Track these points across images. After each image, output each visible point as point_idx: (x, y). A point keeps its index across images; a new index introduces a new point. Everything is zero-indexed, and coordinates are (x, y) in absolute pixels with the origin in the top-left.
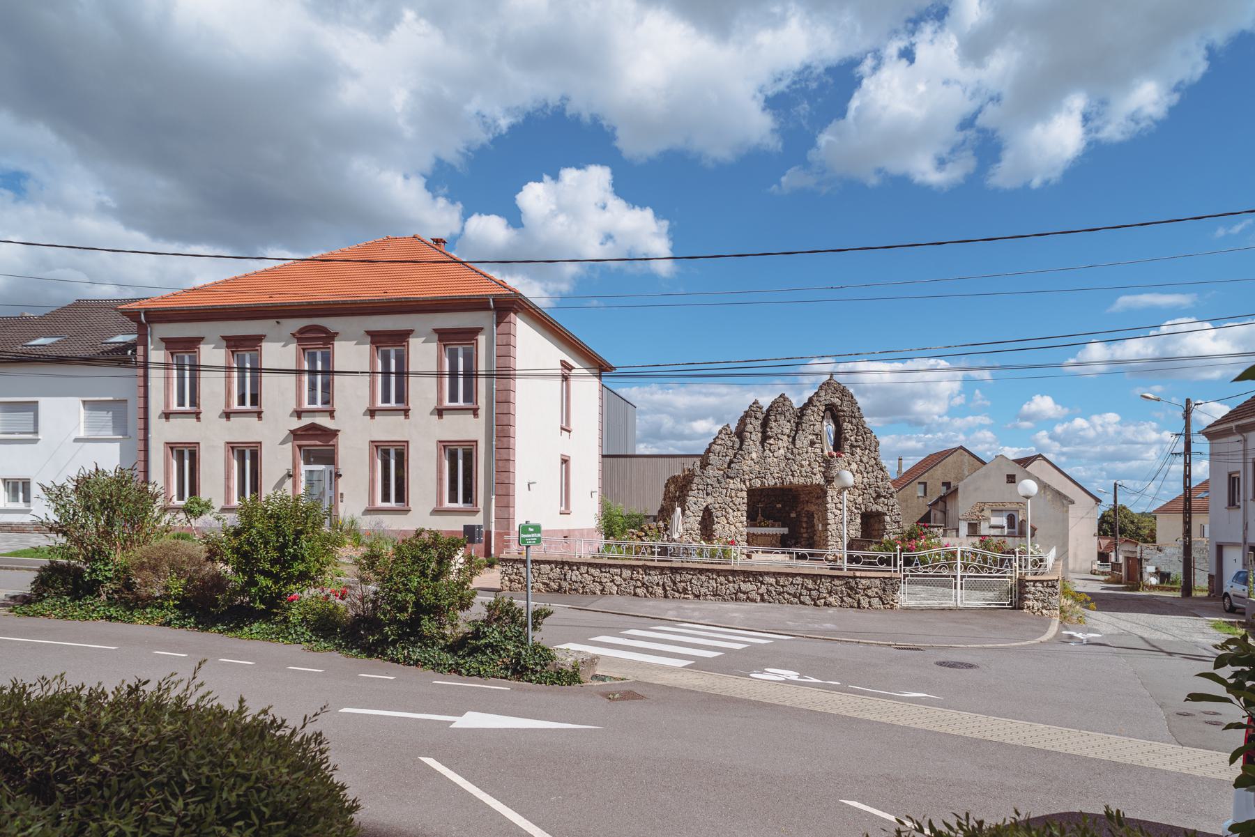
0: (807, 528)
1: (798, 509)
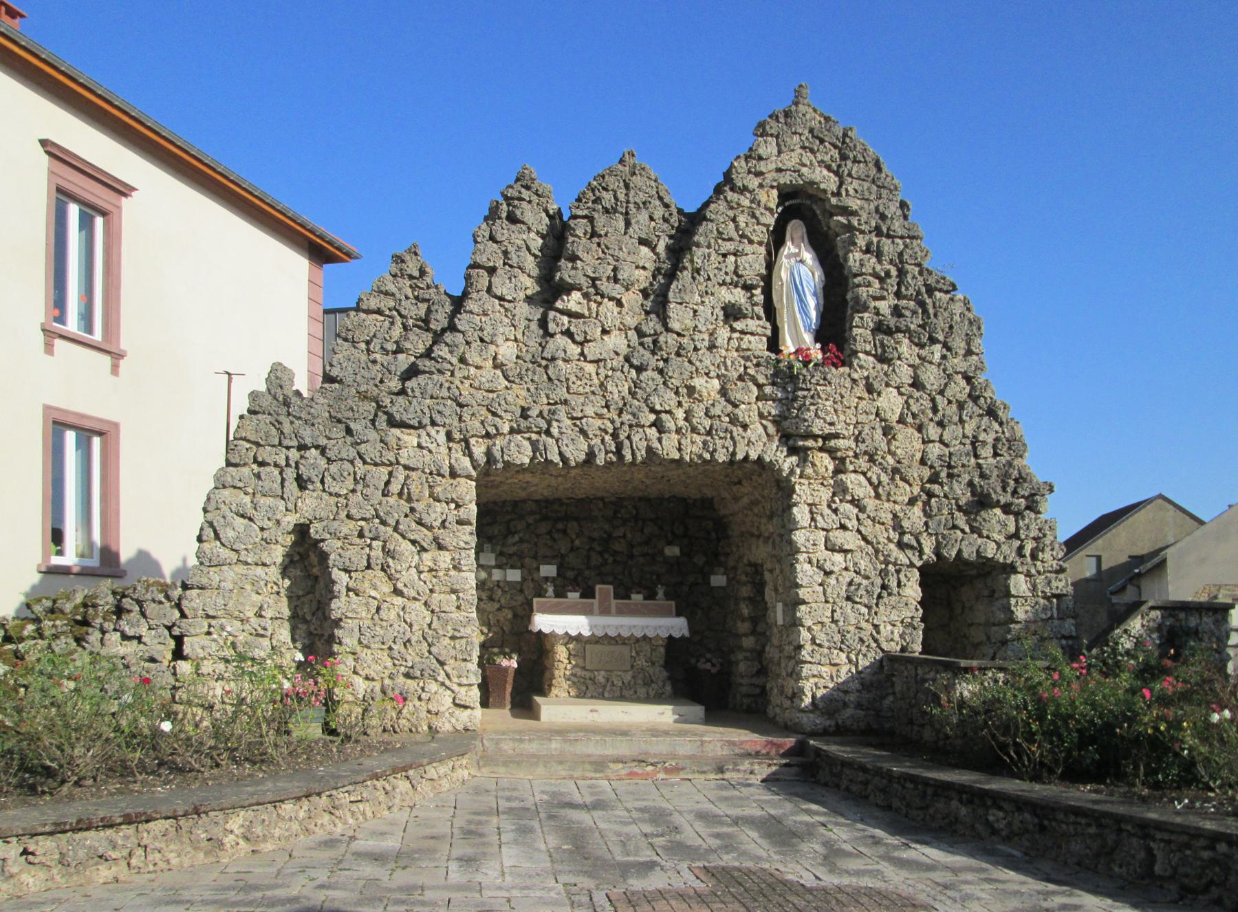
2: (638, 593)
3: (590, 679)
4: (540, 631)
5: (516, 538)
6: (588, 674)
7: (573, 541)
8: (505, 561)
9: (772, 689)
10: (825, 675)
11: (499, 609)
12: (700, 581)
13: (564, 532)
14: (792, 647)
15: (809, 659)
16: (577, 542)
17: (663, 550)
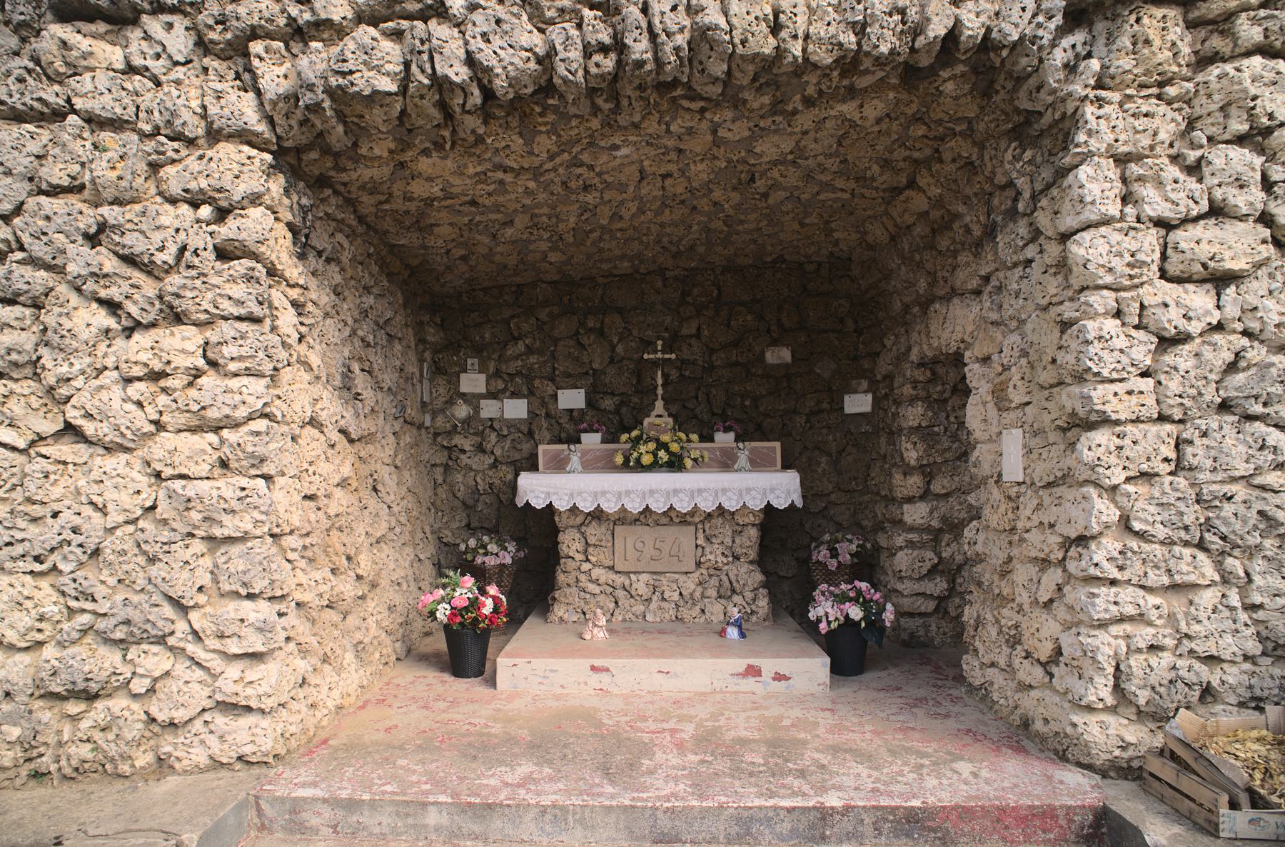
0: (928, 472)
1: (883, 367)
2: (727, 430)
3: (624, 588)
4: (528, 504)
5: (521, 347)
6: (620, 580)
7: (613, 348)
8: (501, 385)
9: (979, 623)
10: (1153, 615)
11: (494, 466)
12: (825, 405)
13: (601, 333)
14: (1054, 540)
15: (1114, 573)
16: (620, 349)
17: (763, 353)
